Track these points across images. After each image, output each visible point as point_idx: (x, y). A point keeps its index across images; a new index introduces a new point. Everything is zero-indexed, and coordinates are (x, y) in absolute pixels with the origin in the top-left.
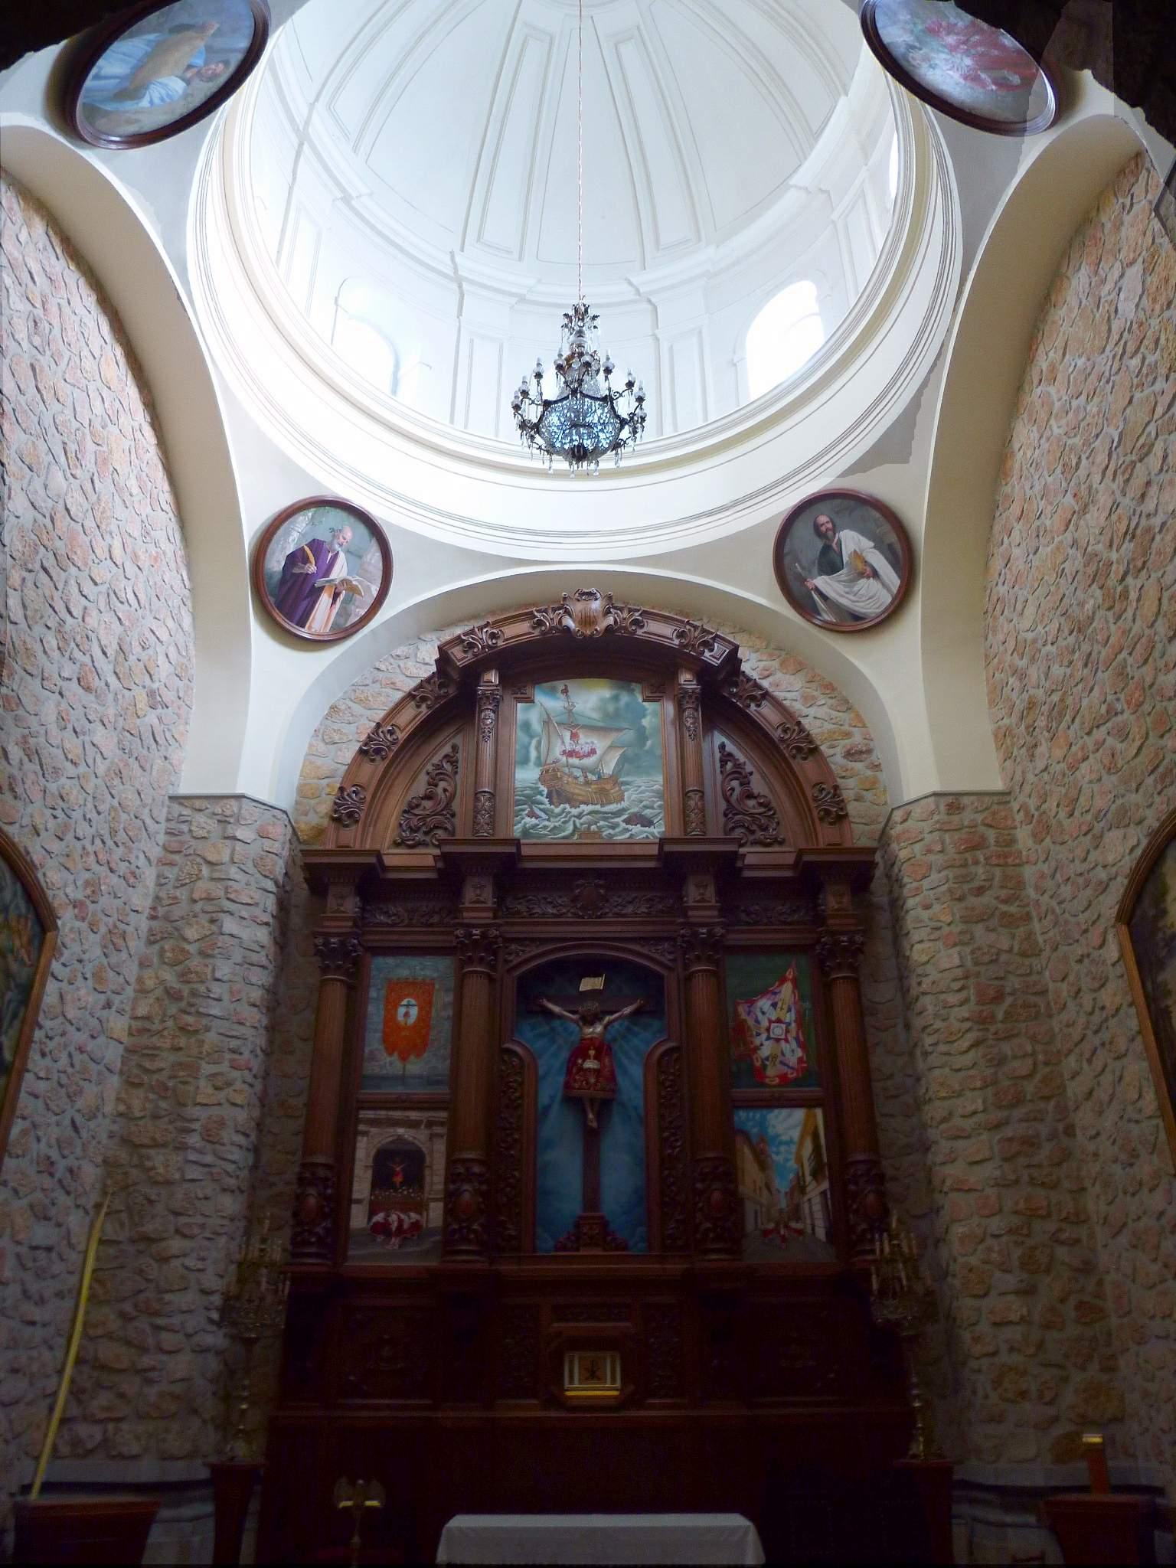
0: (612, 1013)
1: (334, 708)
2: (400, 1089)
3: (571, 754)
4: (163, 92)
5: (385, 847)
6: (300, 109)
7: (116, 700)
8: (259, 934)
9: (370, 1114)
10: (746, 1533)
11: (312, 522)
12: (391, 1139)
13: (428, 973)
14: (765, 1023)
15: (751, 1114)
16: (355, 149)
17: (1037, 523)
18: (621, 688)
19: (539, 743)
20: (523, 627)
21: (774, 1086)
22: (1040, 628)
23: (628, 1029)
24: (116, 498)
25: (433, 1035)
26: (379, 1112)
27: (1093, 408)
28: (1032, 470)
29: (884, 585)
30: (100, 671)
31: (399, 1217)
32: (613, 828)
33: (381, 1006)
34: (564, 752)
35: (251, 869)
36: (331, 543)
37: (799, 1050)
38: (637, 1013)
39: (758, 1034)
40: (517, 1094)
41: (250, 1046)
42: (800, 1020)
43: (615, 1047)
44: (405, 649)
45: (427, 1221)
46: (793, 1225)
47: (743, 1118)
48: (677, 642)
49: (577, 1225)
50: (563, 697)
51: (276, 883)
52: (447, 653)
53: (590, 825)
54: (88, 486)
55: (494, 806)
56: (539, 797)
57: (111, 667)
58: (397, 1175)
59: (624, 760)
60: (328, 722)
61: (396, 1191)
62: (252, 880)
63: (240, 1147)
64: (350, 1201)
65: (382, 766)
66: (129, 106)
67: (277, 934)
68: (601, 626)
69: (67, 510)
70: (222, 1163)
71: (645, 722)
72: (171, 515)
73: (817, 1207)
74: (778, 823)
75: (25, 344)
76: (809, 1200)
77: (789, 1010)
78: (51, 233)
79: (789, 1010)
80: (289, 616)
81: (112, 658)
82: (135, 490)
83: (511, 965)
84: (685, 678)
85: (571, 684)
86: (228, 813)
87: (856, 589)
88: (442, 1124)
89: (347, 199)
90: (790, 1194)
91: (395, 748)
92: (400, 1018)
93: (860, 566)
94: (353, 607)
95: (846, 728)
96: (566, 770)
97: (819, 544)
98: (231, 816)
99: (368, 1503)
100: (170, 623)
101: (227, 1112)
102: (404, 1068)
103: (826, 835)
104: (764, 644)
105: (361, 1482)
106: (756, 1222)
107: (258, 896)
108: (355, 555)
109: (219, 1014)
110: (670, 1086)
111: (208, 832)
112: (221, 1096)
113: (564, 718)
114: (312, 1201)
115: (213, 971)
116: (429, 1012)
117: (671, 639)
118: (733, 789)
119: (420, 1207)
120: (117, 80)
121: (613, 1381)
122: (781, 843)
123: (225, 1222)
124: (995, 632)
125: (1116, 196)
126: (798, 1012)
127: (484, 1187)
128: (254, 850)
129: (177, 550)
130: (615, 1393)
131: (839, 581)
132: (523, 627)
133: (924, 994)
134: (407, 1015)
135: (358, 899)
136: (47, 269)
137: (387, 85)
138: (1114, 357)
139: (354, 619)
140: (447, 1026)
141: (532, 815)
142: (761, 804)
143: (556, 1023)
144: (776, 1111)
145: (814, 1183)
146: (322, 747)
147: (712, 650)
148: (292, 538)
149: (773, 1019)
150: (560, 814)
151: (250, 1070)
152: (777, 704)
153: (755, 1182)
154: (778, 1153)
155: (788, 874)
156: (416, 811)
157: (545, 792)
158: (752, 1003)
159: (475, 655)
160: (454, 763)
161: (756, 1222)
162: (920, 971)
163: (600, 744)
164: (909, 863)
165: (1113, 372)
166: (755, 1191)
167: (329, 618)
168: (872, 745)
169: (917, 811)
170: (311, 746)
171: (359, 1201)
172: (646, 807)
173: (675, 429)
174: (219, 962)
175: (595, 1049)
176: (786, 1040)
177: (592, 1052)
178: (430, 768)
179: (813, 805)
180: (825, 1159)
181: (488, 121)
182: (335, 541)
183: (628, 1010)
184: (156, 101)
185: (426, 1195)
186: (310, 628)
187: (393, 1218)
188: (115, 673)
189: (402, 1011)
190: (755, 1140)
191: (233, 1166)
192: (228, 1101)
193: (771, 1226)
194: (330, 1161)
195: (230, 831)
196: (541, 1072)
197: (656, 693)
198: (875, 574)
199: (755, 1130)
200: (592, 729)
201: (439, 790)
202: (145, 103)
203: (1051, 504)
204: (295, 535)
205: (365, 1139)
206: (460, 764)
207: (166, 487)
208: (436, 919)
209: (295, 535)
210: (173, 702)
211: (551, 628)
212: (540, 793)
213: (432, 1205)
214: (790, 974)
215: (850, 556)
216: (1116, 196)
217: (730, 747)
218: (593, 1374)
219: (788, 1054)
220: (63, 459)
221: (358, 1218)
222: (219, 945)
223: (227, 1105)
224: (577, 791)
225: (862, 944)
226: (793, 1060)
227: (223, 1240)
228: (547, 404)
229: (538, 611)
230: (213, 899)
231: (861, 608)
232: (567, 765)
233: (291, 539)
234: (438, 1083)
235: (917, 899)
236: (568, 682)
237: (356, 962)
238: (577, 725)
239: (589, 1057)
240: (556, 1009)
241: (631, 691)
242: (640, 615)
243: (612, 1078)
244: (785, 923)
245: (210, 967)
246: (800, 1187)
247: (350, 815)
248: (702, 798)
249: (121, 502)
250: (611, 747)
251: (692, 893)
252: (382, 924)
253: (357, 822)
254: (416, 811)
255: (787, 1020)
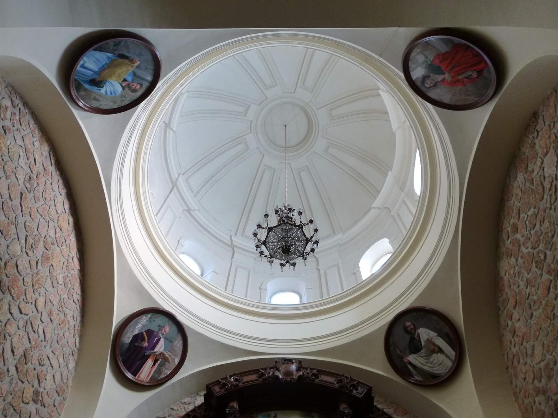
4: (112, 89)
6: (175, 175)
7: (11, 383)
11: (150, 320)
16: (195, 196)
17: (528, 301)
20: (254, 377)
22: (548, 357)
24: (49, 278)
27: (546, 224)
28: (517, 278)
29: (447, 356)
30: (6, 360)
36: (158, 333)
48: (337, 385)
54: (34, 264)
57: (15, 362)
66: (95, 89)
69: (17, 266)
72: (78, 306)
75: (21, 182)
78: (51, 153)
81: (17, 357)
82: (61, 282)
87: (431, 360)
89: (189, 210)
93: (432, 347)
94: (164, 369)
97: (407, 338)
100: (61, 360)
108: (169, 340)
117: (334, 384)
120: (92, 73)
124: (516, 376)
125: (527, 137)
129: (76, 326)
131: (422, 357)
132: (254, 377)
136: (45, 165)
137: (209, 180)
138: (551, 195)
139: (163, 376)
147: (357, 390)
148: (138, 327)
159: (226, 390)
165: (552, 202)
167: (150, 372)
173: (328, 295)
181: (249, 196)
182: (160, 332)
184: (109, 93)
186: (139, 377)
188: (16, 367)
198: (441, 351)
202: (103, 91)
203: (534, 286)
204: (140, 326)
207: (79, 292)
209: (140, 326)
210: (49, 405)
215: (425, 342)
216: (527, 137)
220: (23, 241)
228: (270, 229)
229: (262, 369)
231: (437, 370)
233: (137, 327)
242: (317, 371)
249: (50, 282)
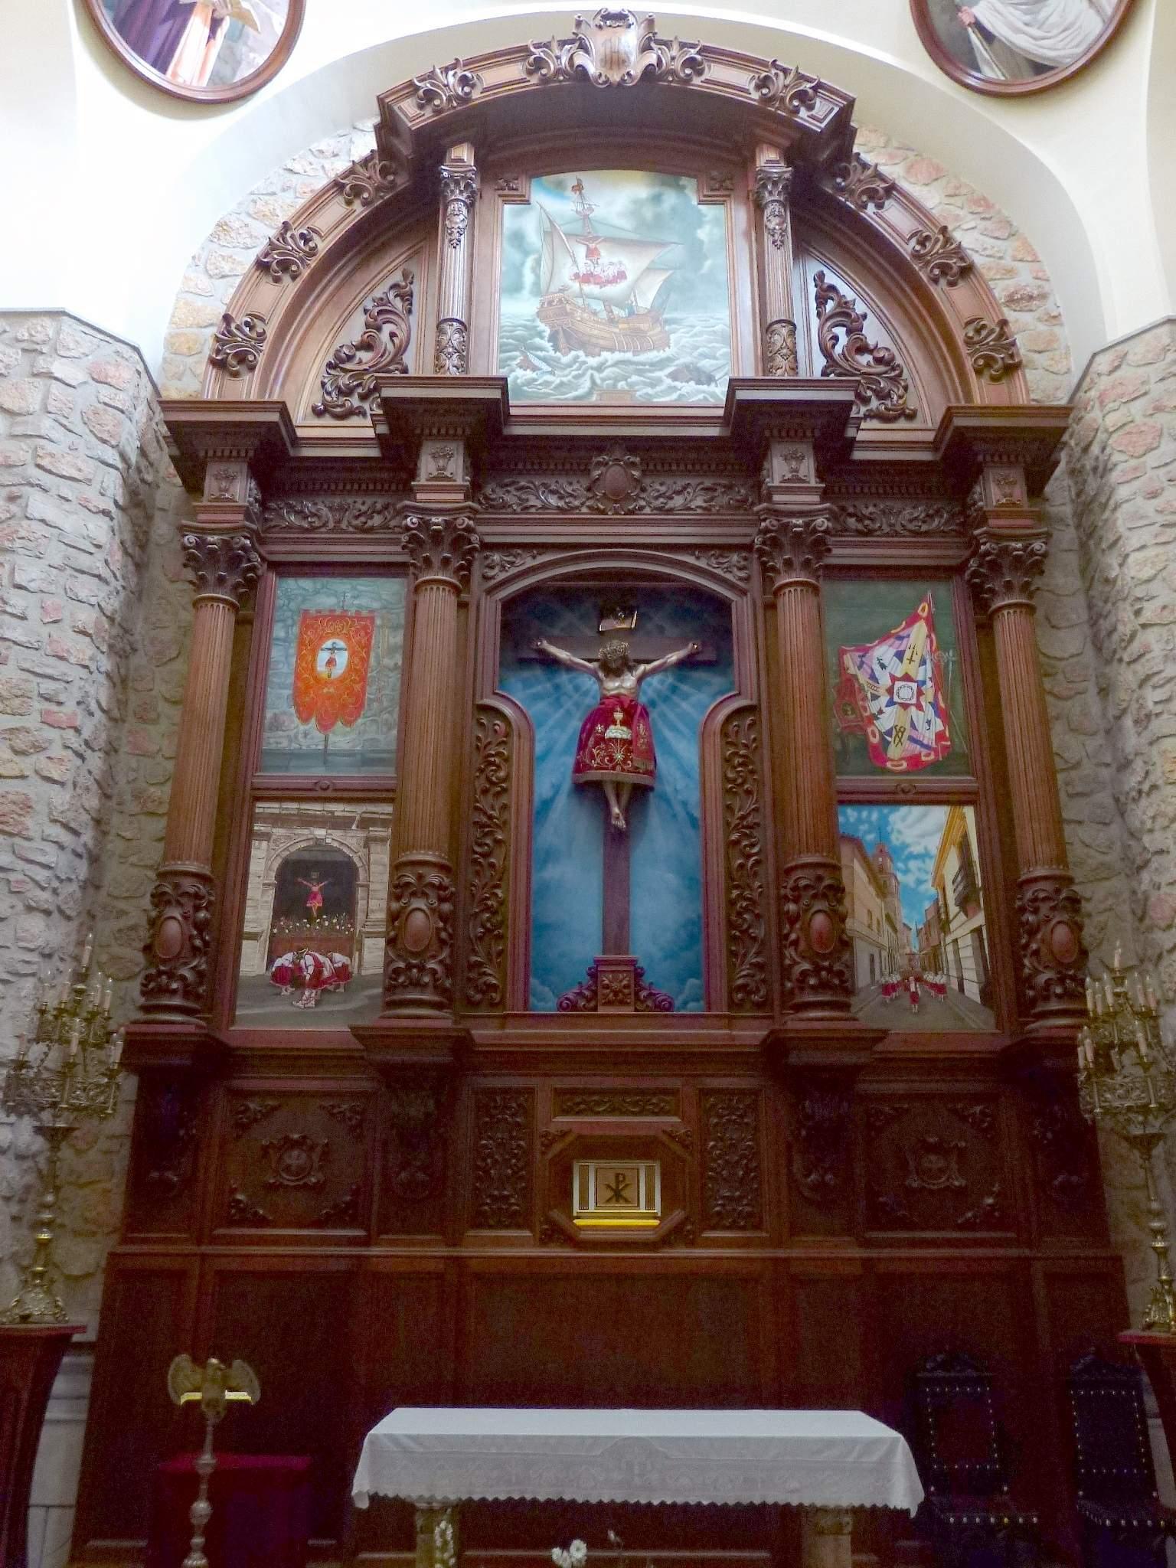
0: (648, 662)
1: (223, 226)
2: (319, 771)
3: (587, 278)
5: (300, 415)
8: (91, 526)
9: (273, 808)
10: (891, 1452)
12: (303, 845)
13: (363, 601)
14: (885, 681)
15: (865, 814)
18: (663, 184)
19: (538, 262)
21: (901, 773)
23: (674, 689)
25: (371, 692)
26: (285, 805)
31: (315, 959)
32: (653, 385)
33: (292, 651)
34: (577, 276)
35: (79, 427)
37: (939, 721)
38: (687, 664)
39: (875, 697)
40: (502, 774)
41: (78, 695)
42: (939, 677)
43: (654, 714)
44: (332, 142)
45: (360, 965)
46: (930, 977)
47: (852, 820)
49: (594, 975)
50: (575, 196)
51: (123, 457)
52: (390, 108)
53: (616, 380)
55: (465, 343)
56: (537, 340)
58: (315, 897)
59: (667, 289)
60: (215, 246)
61: (311, 920)
62: (80, 443)
63: (62, 847)
64: (241, 936)
65: (290, 288)
67: (128, 537)
68: (636, 69)
70: (27, 866)
71: (703, 234)
73: (967, 953)
74: (906, 388)
76: (955, 941)
77: (923, 662)
79: (923, 662)
80: (141, 50)
83: (492, 582)
84: (769, 160)
85: (587, 178)
86: (39, 337)
88: (384, 823)
90: (925, 932)
91: (313, 263)
92: (321, 667)
94: (244, 49)
95: (1008, 262)
96: (580, 301)
98: (44, 342)
99: (230, 1396)
101: (34, 789)
102: (326, 740)
103: (984, 392)
104: (882, 141)
105: (214, 1361)
106: (872, 971)
107: (89, 468)
109: (21, 639)
110: (740, 765)
111: (7, 367)
112: (26, 765)
113: (577, 227)
114: (173, 929)
115: (12, 572)
116: (365, 661)
117: (747, 91)
118: (836, 338)
119: (350, 944)
121: (650, 1203)
122: (911, 417)
123: (34, 957)
126: (936, 667)
127: (446, 907)
128: (89, 395)
130: (656, 1222)
132: (514, 71)
133: (1144, 626)
134: (331, 662)
135: (253, 484)
139: (245, 72)
140: (394, 679)
141: (526, 365)
142: (879, 361)
143: (564, 678)
144: (904, 810)
145: (962, 917)
146: (204, 282)
147: (811, 108)
149: (899, 675)
150: (569, 365)
151: (77, 730)
152: (912, 205)
153: (870, 913)
154: (906, 871)
155: (925, 456)
156: (348, 366)
157: (547, 333)
158: (866, 651)
159: (438, 111)
160: (407, 297)
161: (872, 971)
162: (1139, 592)
163: (632, 264)
164: (1120, 433)
166: (869, 926)
168: (1047, 287)
169: (1138, 351)
170: (186, 279)
171: (254, 937)
172: (704, 356)
174: (21, 560)
175: (623, 710)
176: (919, 707)
177: (619, 716)
178: (369, 305)
179: (964, 350)
180: (979, 882)
183: (673, 657)
185: (359, 928)
187: (308, 960)
189: (323, 656)
190: (871, 852)
191: (46, 873)
192: (37, 772)
193: (895, 978)
194: (206, 870)
195: (42, 364)
196: (539, 748)
197: (718, 190)
199: (870, 837)
200: (619, 242)
201: (384, 336)
205: (264, 843)
206: (415, 300)
208: (377, 520)
211: (558, 71)
212: (540, 335)
213: (368, 942)
214: (923, 609)
217: (831, 279)
218: (617, 1194)
219: (920, 724)
221: (252, 961)
222: (23, 533)
223: (35, 779)
224: (596, 332)
225: (1045, 555)
226: (929, 737)
227: (29, 984)
230: (10, 466)
231: (1046, 49)
232: (581, 295)
234: (381, 762)
235: (1136, 484)
236: (581, 175)
237: (252, 584)
238: (597, 238)
239: (614, 722)
240: (563, 654)
241: (681, 189)
242: (698, 53)
243: (650, 755)
244: (916, 533)
245: (7, 566)
246: (941, 922)
247: (241, 358)
248: (793, 333)
250: (650, 269)
251: (778, 469)
252: (290, 528)
253: (252, 369)
254: (348, 366)
255: (920, 678)
